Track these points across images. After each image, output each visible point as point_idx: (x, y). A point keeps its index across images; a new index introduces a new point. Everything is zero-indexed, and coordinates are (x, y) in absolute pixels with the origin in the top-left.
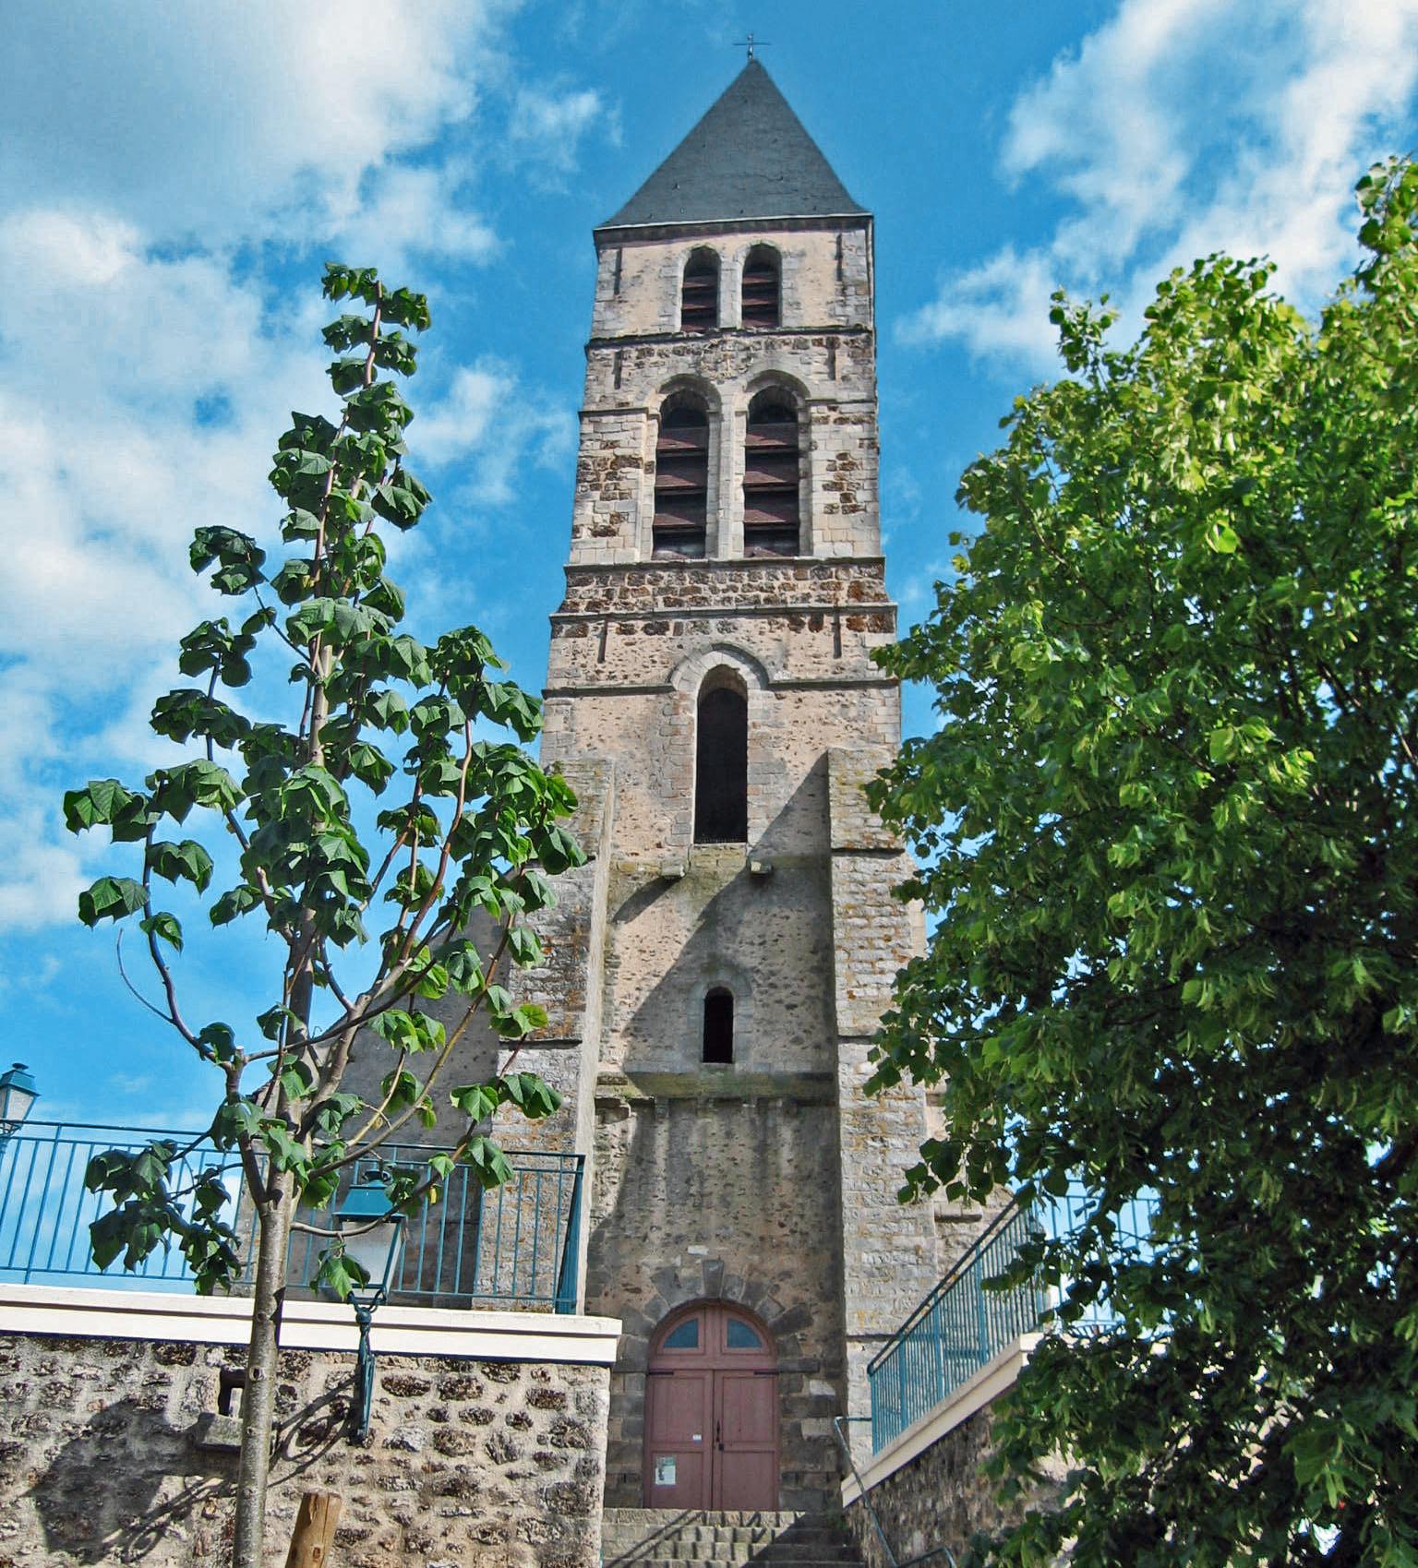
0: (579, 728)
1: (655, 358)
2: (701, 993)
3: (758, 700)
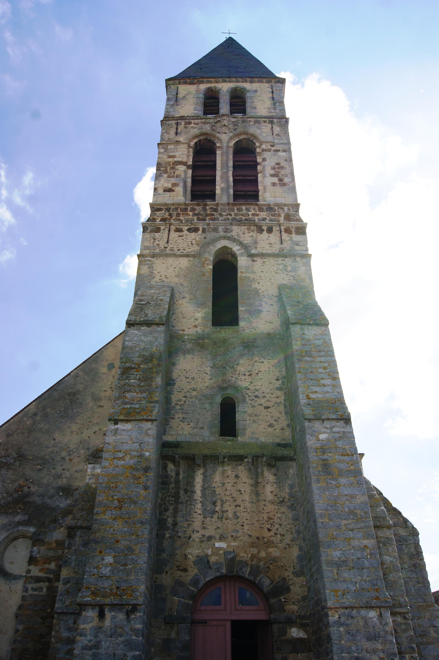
0: (155, 272)
1: (192, 125)
2: (219, 399)
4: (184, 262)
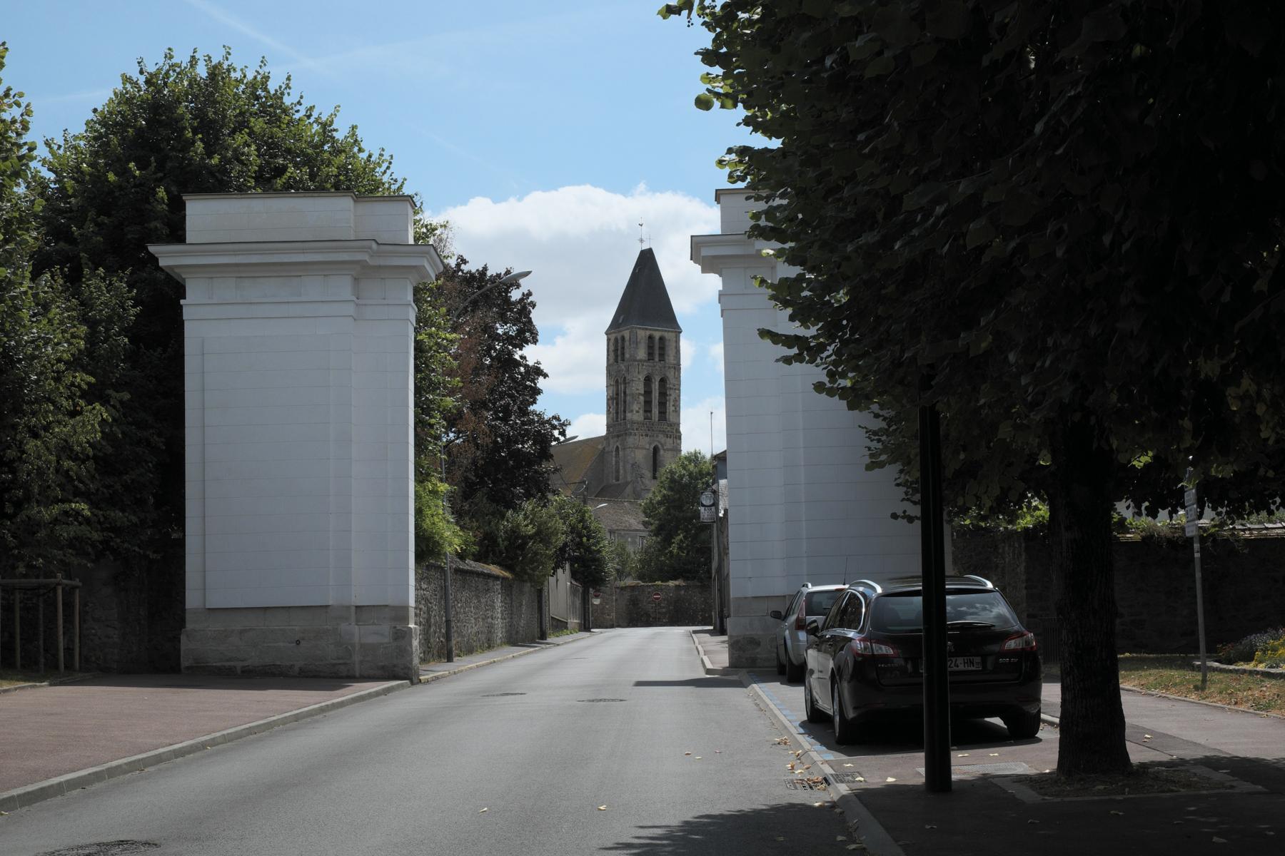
3: (662, 452)
4: (644, 452)
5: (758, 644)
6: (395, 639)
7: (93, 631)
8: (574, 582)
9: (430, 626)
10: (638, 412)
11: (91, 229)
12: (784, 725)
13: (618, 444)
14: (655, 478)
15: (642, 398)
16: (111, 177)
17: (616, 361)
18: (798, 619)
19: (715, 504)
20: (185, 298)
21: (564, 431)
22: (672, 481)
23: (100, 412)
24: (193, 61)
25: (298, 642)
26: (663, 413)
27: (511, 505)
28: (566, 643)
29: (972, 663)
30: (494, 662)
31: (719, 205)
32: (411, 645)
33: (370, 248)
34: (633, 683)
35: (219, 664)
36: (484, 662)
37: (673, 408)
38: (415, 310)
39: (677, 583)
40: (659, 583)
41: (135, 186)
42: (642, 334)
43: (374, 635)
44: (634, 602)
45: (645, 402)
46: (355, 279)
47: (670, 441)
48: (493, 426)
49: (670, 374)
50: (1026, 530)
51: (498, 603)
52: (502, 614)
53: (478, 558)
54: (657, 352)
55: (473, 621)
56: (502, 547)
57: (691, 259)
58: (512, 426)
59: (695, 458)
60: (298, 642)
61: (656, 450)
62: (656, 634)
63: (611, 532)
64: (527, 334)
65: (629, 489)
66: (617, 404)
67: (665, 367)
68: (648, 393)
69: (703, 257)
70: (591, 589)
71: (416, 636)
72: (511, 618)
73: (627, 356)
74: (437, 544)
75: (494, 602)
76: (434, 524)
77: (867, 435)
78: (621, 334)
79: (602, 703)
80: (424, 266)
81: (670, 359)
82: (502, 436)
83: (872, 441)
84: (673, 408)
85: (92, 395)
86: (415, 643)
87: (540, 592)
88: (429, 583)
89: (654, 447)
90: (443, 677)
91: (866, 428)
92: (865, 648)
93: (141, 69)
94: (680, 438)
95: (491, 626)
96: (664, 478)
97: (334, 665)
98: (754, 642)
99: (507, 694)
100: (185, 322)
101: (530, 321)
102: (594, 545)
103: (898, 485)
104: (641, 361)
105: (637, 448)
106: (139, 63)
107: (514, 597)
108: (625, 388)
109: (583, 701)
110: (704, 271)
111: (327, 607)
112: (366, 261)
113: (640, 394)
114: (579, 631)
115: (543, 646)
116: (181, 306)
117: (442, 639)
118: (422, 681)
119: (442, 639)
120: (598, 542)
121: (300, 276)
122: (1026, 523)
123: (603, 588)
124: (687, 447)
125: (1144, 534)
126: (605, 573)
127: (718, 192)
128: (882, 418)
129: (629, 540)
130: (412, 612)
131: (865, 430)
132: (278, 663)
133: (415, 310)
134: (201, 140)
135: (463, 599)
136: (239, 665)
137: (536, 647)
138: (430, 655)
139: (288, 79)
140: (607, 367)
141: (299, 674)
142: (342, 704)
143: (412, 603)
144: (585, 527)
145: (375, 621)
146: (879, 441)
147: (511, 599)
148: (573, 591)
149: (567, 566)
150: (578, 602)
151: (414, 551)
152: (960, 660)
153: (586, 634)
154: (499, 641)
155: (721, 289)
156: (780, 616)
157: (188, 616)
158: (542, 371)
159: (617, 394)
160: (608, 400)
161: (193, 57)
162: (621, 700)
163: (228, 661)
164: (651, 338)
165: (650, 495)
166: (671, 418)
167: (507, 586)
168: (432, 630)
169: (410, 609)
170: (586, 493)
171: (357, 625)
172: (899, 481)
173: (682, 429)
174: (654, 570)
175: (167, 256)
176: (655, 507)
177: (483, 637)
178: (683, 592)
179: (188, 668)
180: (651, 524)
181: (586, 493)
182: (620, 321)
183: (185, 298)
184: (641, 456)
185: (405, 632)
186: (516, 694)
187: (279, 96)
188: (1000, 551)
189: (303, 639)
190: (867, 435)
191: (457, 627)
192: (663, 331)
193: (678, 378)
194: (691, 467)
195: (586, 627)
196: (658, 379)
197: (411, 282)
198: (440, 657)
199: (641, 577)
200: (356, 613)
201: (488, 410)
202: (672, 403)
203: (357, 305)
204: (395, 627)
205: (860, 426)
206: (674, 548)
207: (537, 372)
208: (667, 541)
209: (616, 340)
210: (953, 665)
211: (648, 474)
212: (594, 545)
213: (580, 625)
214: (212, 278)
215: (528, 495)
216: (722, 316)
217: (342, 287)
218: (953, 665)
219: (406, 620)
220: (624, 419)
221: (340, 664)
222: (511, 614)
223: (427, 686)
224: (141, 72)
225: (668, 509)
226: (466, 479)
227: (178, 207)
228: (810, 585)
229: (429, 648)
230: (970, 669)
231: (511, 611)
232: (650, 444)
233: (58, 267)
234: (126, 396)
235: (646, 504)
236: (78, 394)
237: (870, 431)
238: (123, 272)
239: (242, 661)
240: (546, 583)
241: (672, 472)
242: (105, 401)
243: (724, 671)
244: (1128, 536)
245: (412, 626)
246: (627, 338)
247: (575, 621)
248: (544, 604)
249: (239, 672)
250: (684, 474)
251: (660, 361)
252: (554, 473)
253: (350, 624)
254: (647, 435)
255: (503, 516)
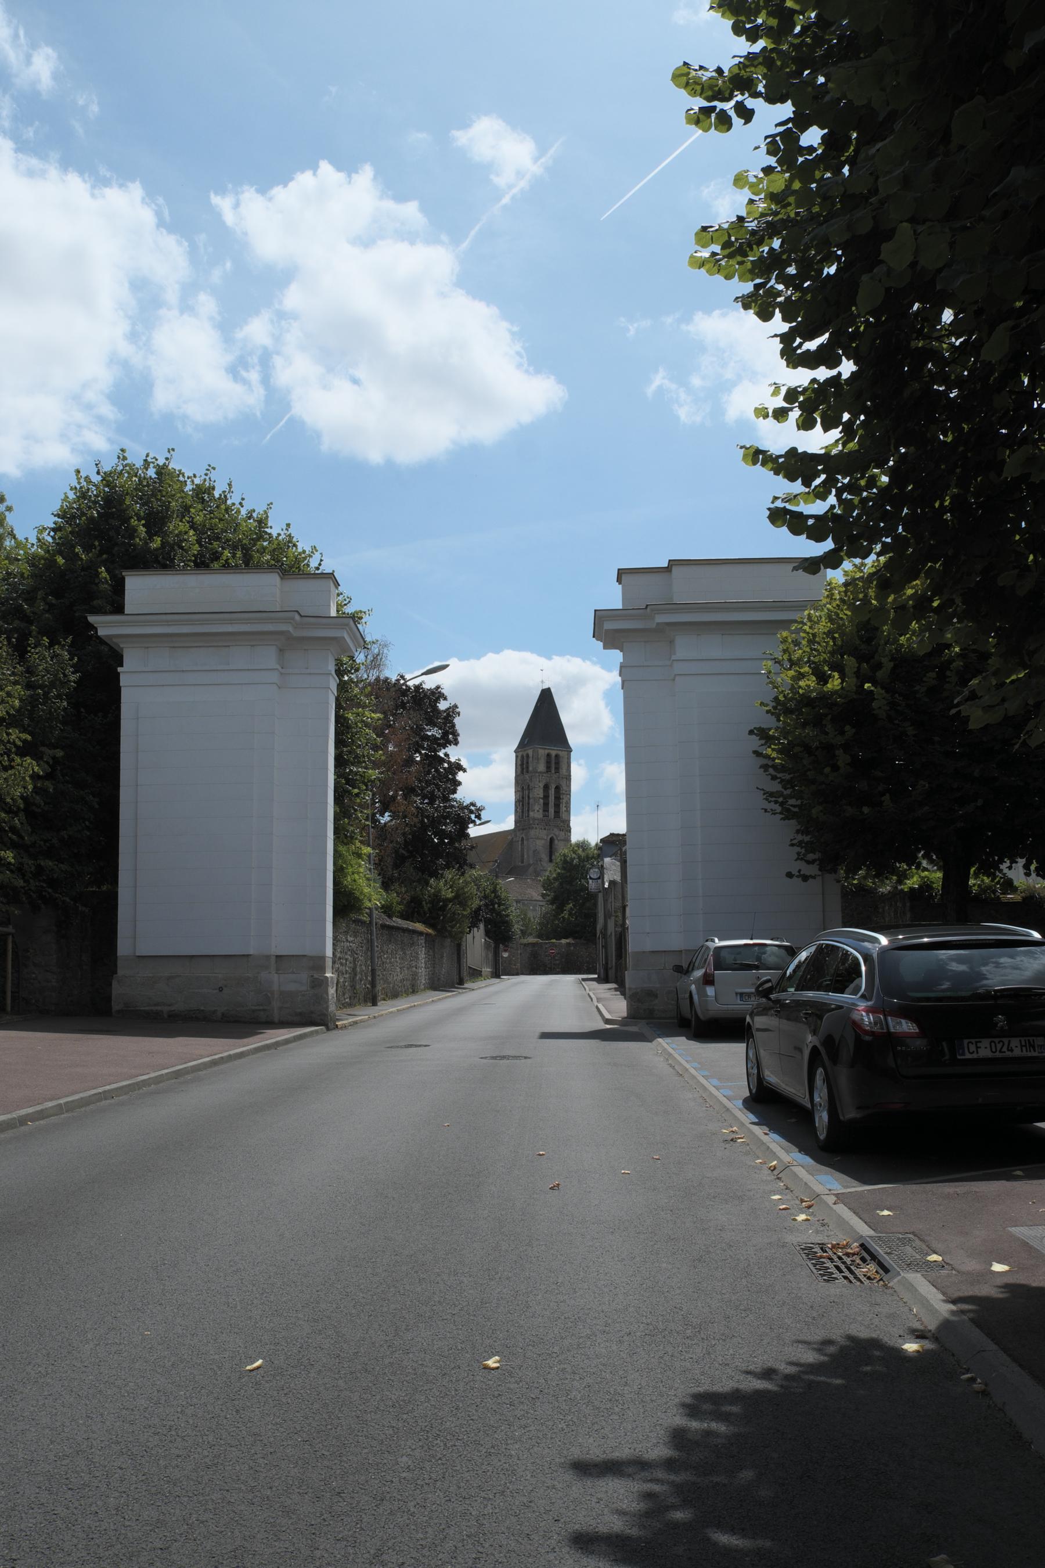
3: (556, 842)
4: (543, 842)
5: (656, 996)
6: (313, 987)
7: (34, 976)
8: (487, 939)
9: (356, 975)
10: (538, 811)
11: (42, 608)
12: (725, 1107)
13: (523, 836)
14: (551, 861)
15: (541, 801)
16: (60, 560)
17: (522, 772)
18: (705, 974)
19: (601, 877)
20: (122, 666)
21: (480, 815)
22: (565, 862)
23: (30, 765)
24: (146, 464)
25: (221, 989)
26: (557, 813)
27: (435, 874)
28: (480, 988)
29: (1032, 1046)
30: (415, 1006)
31: (621, 586)
32: (327, 994)
33: (293, 619)
34: (537, 1034)
35: (147, 1008)
36: (406, 1006)
37: (565, 809)
38: (336, 681)
39: (568, 941)
40: (554, 941)
41: (83, 569)
42: (542, 752)
43: (294, 982)
44: (534, 955)
45: (544, 804)
46: (281, 650)
47: (563, 833)
48: (421, 809)
49: (563, 783)
50: (912, 889)
51: (422, 955)
52: (426, 964)
53: (405, 916)
54: (553, 766)
55: (399, 970)
56: (426, 908)
57: (594, 637)
58: (436, 809)
59: (583, 845)
60: (221, 989)
61: (552, 840)
62: (553, 980)
63: (518, 901)
64: (450, 736)
65: (531, 869)
66: (523, 805)
67: (559, 778)
68: (546, 797)
69: (607, 631)
70: (501, 945)
71: (333, 983)
72: (434, 968)
73: (531, 769)
74: (358, 900)
75: (417, 954)
76: (355, 881)
77: (765, 797)
78: (526, 752)
79: (505, 1061)
80: (344, 638)
81: (563, 771)
82: (428, 817)
83: (770, 802)
84: (564, 809)
85: (24, 750)
86: (332, 991)
87: (459, 946)
88: (355, 936)
89: (551, 839)
90: (361, 1021)
91: (763, 790)
92: (876, 1023)
93: (99, 470)
94: (570, 832)
95: (415, 975)
96: (558, 860)
97: (254, 1011)
98: (651, 994)
99: (411, 1046)
100: (122, 689)
101: (453, 726)
102: (504, 910)
103: (792, 845)
104: (540, 772)
105: (538, 838)
106: (97, 465)
107: (436, 950)
108: (529, 793)
109: (486, 1058)
110: (605, 648)
111: (248, 956)
112: (289, 631)
113: (540, 798)
114: (492, 977)
115: (460, 991)
116: (119, 674)
117: (368, 986)
118: (339, 1027)
119: (368, 986)
120: (507, 908)
121: (229, 646)
122: (913, 884)
123: (511, 945)
124: (575, 837)
125: (1023, 895)
126: (512, 932)
127: (620, 571)
128: (779, 780)
129: (531, 908)
130: (329, 963)
131: (762, 792)
132: (202, 1008)
133: (336, 681)
134: (143, 525)
135: (389, 951)
136: (166, 1009)
137: (454, 991)
138: (356, 1000)
139: (230, 485)
140: (516, 777)
141: (222, 1019)
142: (241, 1055)
143: (329, 952)
144: (497, 897)
145: (294, 970)
146: (776, 802)
147: (434, 951)
148: (487, 946)
149: (482, 926)
150: (491, 955)
151: (332, 904)
152: (1015, 1042)
153: (497, 980)
154: (422, 987)
155: (622, 661)
156: (683, 971)
157: (119, 963)
158: (443, 694)
159: (523, 798)
160: (516, 802)
161: (145, 460)
162: (526, 1058)
163: (155, 1005)
164: (549, 755)
165: (547, 873)
166: (564, 816)
167: (430, 940)
168: (358, 978)
169: (327, 959)
170: (497, 870)
171: (276, 973)
172: (794, 842)
173: (572, 824)
174: (550, 930)
175: (105, 626)
176: (551, 883)
177: (407, 983)
178: (572, 948)
179: (119, 1012)
180: (549, 896)
181: (497, 870)
182: (526, 742)
183: (122, 666)
184: (541, 845)
185: (322, 981)
186: (420, 1046)
187: (223, 499)
188: (881, 910)
189: (226, 986)
190: (765, 797)
191: (383, 975)
192: (557, 750)
193: (569, 786)
194: (580, 852)
195: (496, 975)
196: (554, 786)
197: (332, 653)
198: (365, 1001)
199: (540, 936)
200: (276, 962)
201: (417, 796)
202: (564, 805)
203: (282, 674)
204: (312, 976)
205: (757, 788)
206: (565, 914)
207: (458, 767)
208: (560, 908)
209: (522, 757)
210: (1005, 1049)
211: (545, 857)
212: (504, 910)
213: (492, 973)
214: (148, 648)
215: (448, 866)
216: (622, 688)
217: (267, 656)
218: (1005, 1049)
219: (323, 969)
220: (528, 816)
221: (260, 1010)
222: (434, 964)
223: (345, 1032)
224: (98, 473)
225: (561, 884)
226: (396, 852)
227: (119, 588)
228: (716, 940)
229: (355, 993)
230: (1029, 1054)
231: (433, 961)
232: (547, 836)
233: (5, 636)
234: (59, 753)
235: (544, 880)
236: (13, 751)
237: (767, 793)
238: (64, 641)
239: (169, 1006)
240: (464, 939)
241: (564, 855)
242: (38, 757)
243: (624, 1022)
244: (1009, 896)
245: (328, 975)
246: (531, 755)
247: (488, 970)
248: (462, 956)
249: (166, 1016)
250: (574, 858)
251: (555, 773)
252: (471, 850)
253: (270, 973)
254: (545, 829)
255: (427, 883)
